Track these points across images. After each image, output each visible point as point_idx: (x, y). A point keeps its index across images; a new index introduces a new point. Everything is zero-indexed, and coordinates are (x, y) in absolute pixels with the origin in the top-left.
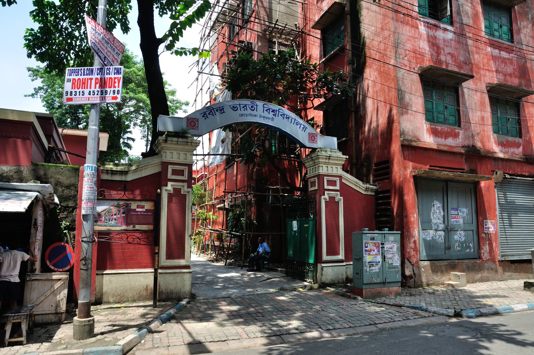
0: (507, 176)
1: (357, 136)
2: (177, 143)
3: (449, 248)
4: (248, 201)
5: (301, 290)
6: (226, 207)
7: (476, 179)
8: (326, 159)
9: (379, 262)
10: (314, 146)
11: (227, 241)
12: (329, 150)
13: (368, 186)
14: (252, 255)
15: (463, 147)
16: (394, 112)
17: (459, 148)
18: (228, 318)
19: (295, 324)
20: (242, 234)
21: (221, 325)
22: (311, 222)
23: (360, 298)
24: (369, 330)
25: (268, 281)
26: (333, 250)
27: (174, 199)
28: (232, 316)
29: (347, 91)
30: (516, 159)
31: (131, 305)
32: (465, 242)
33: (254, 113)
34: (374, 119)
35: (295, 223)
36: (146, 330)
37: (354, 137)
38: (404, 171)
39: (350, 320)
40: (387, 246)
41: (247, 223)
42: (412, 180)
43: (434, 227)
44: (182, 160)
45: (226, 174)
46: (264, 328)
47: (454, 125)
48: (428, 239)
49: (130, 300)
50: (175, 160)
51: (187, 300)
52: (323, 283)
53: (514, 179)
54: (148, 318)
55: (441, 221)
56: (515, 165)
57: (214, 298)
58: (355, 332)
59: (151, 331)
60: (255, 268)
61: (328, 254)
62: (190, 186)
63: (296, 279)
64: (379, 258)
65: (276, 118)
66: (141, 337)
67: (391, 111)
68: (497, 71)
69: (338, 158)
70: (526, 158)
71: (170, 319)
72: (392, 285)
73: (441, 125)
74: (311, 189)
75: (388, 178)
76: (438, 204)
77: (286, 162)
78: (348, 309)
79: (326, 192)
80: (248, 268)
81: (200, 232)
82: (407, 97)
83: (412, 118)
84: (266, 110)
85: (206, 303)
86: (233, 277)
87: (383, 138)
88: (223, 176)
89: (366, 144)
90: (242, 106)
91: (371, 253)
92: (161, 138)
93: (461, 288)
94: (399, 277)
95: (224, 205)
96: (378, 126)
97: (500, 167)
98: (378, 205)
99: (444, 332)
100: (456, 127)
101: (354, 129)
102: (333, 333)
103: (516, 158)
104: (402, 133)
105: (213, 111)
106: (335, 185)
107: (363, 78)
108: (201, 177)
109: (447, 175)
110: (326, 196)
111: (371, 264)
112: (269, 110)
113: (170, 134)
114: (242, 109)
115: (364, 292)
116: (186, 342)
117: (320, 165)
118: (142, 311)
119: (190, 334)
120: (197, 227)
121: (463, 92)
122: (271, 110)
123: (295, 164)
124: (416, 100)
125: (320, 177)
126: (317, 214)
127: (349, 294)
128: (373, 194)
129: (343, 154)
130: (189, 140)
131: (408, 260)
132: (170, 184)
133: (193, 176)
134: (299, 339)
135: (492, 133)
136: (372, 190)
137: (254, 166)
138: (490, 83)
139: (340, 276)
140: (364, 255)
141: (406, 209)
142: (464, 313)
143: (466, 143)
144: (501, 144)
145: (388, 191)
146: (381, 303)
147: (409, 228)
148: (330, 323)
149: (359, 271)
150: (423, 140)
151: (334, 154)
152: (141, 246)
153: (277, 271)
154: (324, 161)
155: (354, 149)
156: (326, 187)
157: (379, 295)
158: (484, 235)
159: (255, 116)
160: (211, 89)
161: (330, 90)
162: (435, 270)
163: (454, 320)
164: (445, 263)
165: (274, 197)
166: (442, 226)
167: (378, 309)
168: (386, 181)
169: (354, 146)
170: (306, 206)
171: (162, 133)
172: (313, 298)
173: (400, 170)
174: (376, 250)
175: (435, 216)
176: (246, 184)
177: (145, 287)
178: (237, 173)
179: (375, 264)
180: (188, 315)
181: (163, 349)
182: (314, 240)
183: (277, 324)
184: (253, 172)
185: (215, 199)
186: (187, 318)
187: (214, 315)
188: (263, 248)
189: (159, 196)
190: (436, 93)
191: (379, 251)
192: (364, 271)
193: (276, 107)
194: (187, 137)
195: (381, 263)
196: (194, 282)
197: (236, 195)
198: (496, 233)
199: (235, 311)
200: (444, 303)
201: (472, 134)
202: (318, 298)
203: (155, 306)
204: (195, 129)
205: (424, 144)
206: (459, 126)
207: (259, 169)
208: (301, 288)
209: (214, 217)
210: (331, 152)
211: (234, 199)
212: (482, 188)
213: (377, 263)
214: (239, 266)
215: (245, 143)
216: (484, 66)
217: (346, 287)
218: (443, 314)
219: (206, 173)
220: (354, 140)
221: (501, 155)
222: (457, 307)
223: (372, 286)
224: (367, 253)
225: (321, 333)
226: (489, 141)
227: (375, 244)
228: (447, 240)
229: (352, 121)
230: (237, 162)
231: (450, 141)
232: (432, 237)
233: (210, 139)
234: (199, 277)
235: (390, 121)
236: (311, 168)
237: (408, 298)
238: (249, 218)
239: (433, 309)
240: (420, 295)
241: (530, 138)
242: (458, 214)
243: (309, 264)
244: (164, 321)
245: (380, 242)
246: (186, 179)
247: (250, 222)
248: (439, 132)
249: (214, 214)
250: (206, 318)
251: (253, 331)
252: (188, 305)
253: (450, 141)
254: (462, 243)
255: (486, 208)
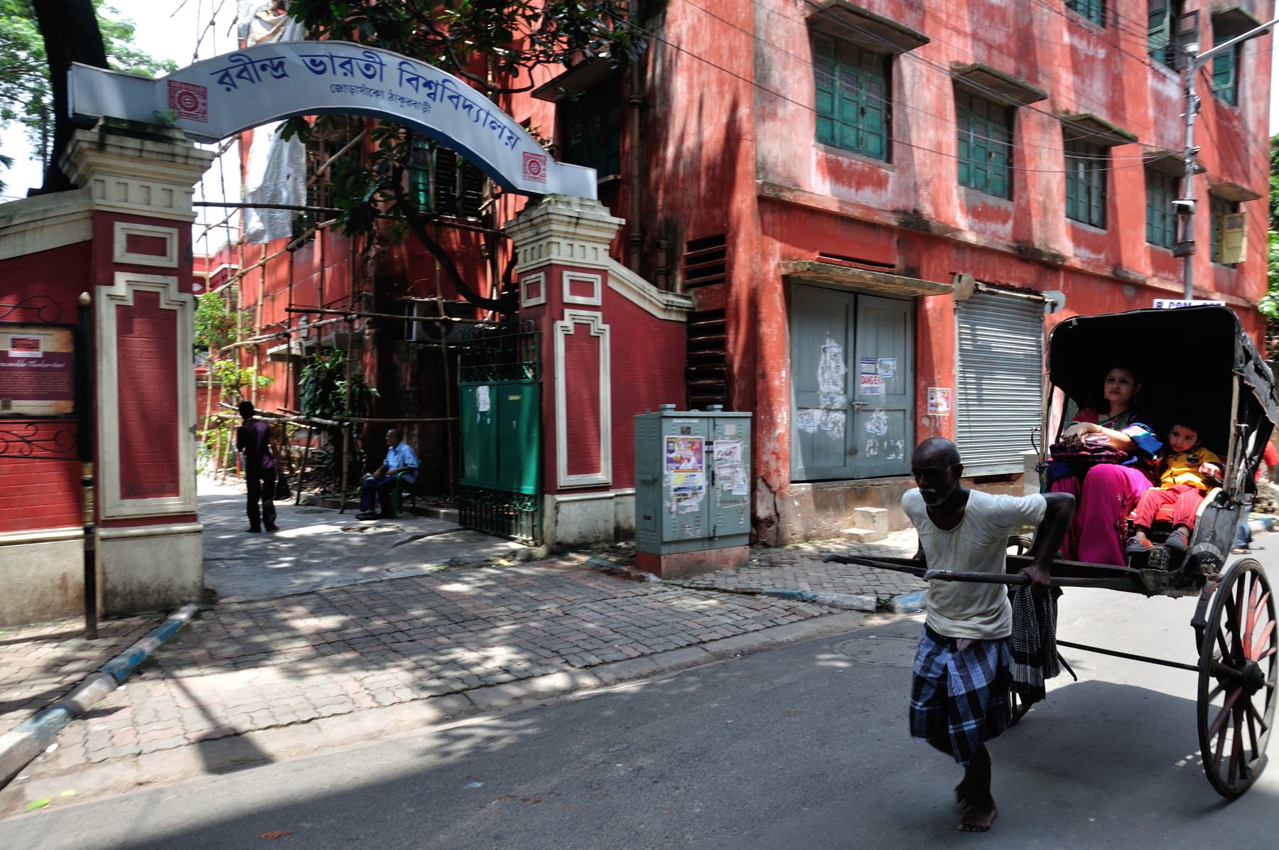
0: (982, 287)
1: (645, 171)
2: (140, 155)
3: (853, 452)
4: (354, 335)
5: (504, 562)
6: (294, 352)
7: (920, 291)
8: (569, 223)
9: (700, 488)
10: (537, 188)
11: (298, 443)
12: (575, 201)
13: (671, 298)
14: (369, 476)
15: (895, 212)
16: (743, 111)
17: (887, 215)
18: (313, 653)
19: (500, 655)
20: (341, 421)
21: (294, 673)
22: (527, 390)
23: (653, 578)
24: (689, 660)
25: (415, 542)
26: (582, 461)
27: (138, 325)
28: (324, 645)
29: (625, 47)
30: (1000, 248)
31: (12, 637)
32: (887, 437)
33: (374, 84)
34: (692, 127)
35: (484, 397)
36: (60, 712)
37: (636, 172)
38: (759, 261)
39: (639, 638)
40: (719, 448)
41: (352, 394)
42: (779, 287)
43: (824, 402)
44: (157, 207)
45: (292, 262)
46: (420, 673)
47: (879, 157)
48: (810, 430)
49: (9, 620)
50: (136, 204)
51: (193, 608)
52: (559, 543)
53: (993, 293)
54: (69, 673)
55: (839, 388)
56: (994, 262)
57: (272, 597)
58: (655, 667)
59: (78, 714)
60: (378, 510)
61: (572, 470)
62: (185, 287)
63: (487, 533)
64: (701, 479)
65: (435, 105)
66: (45, 737)
67: (734, 107)
68: (975, 36)
69: (598, 224)
70: (1019, 249)
71: (141, 668)
72: (730, 542)
73: (849, 153)
74: (526, 303)
75: (722, 281)
76: (833, 348)
77: (455, 236)
78: (630, 608)
79: (567, 312)
80: (358, 511)
81: (223, 419)
82: (776, 76)
83: (785, 131)
84: (409, 80)
85: (247, 614)
86: (319, 535)
87: (711, 179)
88: (283, 271)
89: (667, 191)
90: (338, 62)
91: (683, 466)
92: (85, 137)
93: (876, 543)
94: (745, 524)
95: (289, 349)
96: (700, 146)
97: (968, 265)
98: (692, 346)
99: (868, 653)
100: (882, 163)
101: (636, 151)
102: (602, 674)
103: (1001, 246)
104: (761, 168)
105: (249, 67)
106: (591, 294)
107: (664, 18)
108: (222, 277)
109: (860, 277)
110: (568, 322)
111: (682, 493)
112: (416, 79)
113: (112, 127)
114: (340, 71)
115: (664, 561)
116: (193, 736)
117: (553, 239)
118: (50, 652)
119: (204, 710)
120: (214, 408)
121: (900, 71)
122: (422, 81)
123: (478, 240)
124: (796, 80)
125: (554, 272)
126: (544, 369)
127: (625, 569)
128: (683, 319)
129: (613, 214)
130: (179, 148)
131: (764, 481)
132: (121, 278)
133: (196, 273)
134: (517, 698)
135: (955, 183)
136: (680, 310)
137: (370, 243)
138: (957, 63)
139: (601, 525)
140: (666, 472)
141: (762, 357)
142: (898, 603)
143: (901, 204)
144: (975, 212)
145: (721, 313)
146: (706, 589)
147: (770, 405)
148: (589, 647)
149: (651, 511)
150: (807, 189)
151: (588, 213)
152: (37, 463)
153: (436, 515)
154: (564, 228)
155: (636, 202)
156: (568, 297)
157: (699, 567)
158: (925, 422)
159: (377, 93)
160: (243, 21)
161: (579, 40)
162: (823, 504)
163: (877, 621)
164: (845, 485)
165: (425, 325)
166: (840, 401)
167: (701, 604)
168: (716, 287)
169: (636, 197)
170: (512, 346)
171: (87, 123)
172: (536, 584)
173: (752, 260)
174: (693, 460)
175: (827, 376)
176: (348, 290)
177: (58, 582)
178: (322, 260)
179: (689, 493)
180: (197, 653)
181: (119, 765)
182: (535, 434)
183: (454, 661)
184: (368, 258)
185: (263, 331)
186: (194, 663)
187: (273, 647)
188: (401, 456)
189: (89, 311)
190: (842, 72)
191: (700, 462)
192: (665, 511)
193: (439, 74)
194: (171, 140)
195: (704, 490)
196: (211, 555)
197: (321, 319)
198: (950, 418)
199: (334, 631)
200: (849, 581)
201: (915, 184)
202: (550, 582)
203: (91, 633)
204: (195, 117)
205: (811, 199)
206: (889, 160)
207: (383, 252)
208: (504, 557)
209: (262, 380)
210: (582, 205)
211: (315, 332)
212: (930, 313)
213: (696, 491)
214: (335, 505)
215: (346, 177)
216: (948, 18)
217: (615, 550)
218: (850, 609)
219: (234, 266)
220: (635, 181)
221: (971, 238)
222: (880, 590)
223: (682, 548)
224: (673, 466)
225: (572, 676)
226: (949, 202)
227: (693, 443)
228: (849, 433)
229: (632, 131)
230: (322, 230)
231: (868, 196)
232: (819, 427)
233: (242, 167)
234: (225, 542)
235: (732, 137)
236: (529, 247)
237: (766, 573)
238: (358, 381)
239: (829, 596)
240: (792, 564)
241: (1028, 202)
242: (876, 373)
243: (521, 497)
244: (121, 679)
245: (704, 439)
246: (174, 264)
247: (361, 391)
248: (845, 172)
249: (259, 372)
250: (248, 656)
251: (386, 685)
252: (196, 623)
253: (868, 196)
254: (881, 440)
255: (935, 358)
